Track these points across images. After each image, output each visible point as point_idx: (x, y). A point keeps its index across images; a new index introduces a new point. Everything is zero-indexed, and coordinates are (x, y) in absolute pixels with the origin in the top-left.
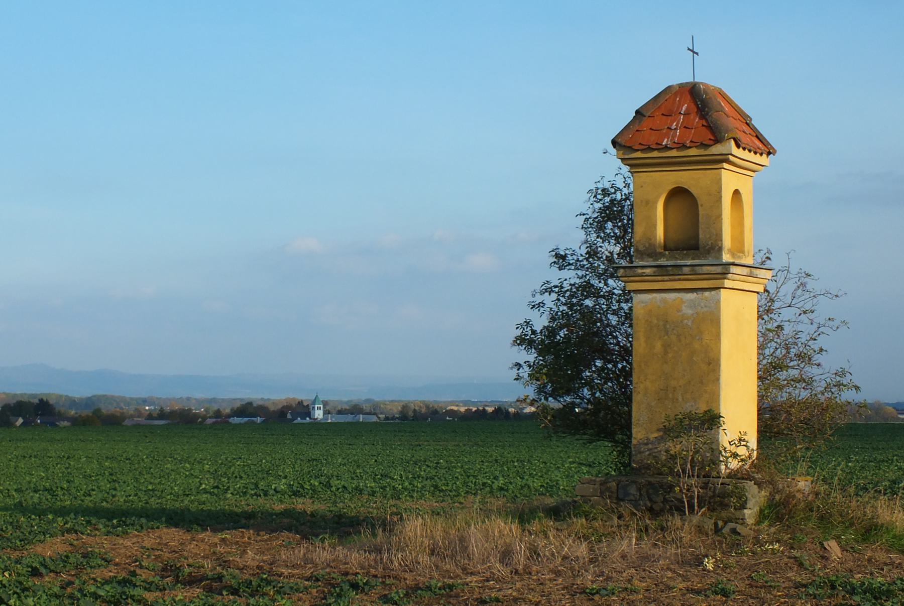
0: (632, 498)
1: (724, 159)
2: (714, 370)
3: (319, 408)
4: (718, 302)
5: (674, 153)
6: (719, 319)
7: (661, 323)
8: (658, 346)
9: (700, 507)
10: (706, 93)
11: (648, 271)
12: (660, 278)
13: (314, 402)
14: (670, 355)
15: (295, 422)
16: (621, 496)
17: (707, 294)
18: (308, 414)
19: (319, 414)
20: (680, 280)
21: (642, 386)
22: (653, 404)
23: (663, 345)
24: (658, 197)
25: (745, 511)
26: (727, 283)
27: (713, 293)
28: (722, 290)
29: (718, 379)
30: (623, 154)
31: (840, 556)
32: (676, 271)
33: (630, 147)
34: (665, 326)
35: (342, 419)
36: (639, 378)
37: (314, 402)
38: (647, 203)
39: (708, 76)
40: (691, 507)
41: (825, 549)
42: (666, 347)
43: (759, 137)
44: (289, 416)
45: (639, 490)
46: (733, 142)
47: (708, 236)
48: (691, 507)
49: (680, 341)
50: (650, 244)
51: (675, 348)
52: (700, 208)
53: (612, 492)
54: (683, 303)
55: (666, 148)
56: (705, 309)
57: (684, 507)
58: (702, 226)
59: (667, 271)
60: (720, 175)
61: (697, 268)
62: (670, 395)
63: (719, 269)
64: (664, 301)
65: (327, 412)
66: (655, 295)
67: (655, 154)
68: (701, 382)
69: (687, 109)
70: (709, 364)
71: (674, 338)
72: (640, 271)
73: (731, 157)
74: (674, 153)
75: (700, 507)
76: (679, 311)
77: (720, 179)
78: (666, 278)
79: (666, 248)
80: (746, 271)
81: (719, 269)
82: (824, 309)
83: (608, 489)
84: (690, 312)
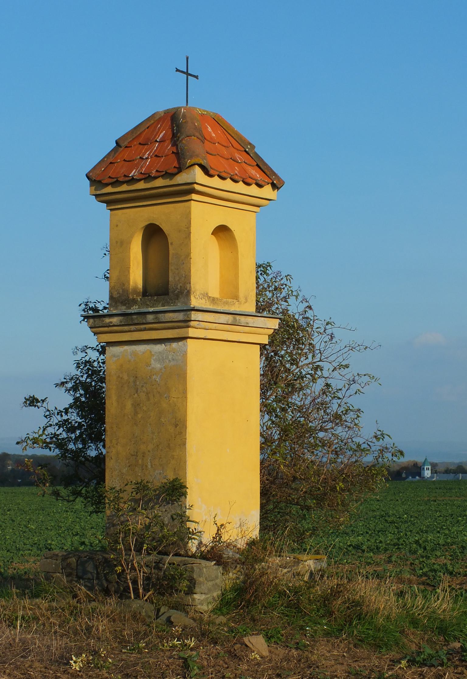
0: (89, 576)
1: (188, 190)
2: (180, 433)
3: (428, 469)
4: (185, 354)
5: (141, 185)
6: (185, 374)
7: (132, 379)
8: (129, 405)
9: (146, 590)
10: (184, 116)
11: (115, 320)
12: (126, 328)
13: (424, 464)
14: (140, 416)
15: (408, 480)
16: (80, 574)
17: (174, 345)
18: (419, 474)
19: (427, 473)
20: (145, 330)
21: (114, 451)
22: (124, 471)
23: (133, 405)
24: (132, 237)
25: (195, 596)
26: (191, 332)
27: (180, 343)
28: (188, 340)
29: (184, 444)
30: (96, 190)
31: (266, 653)
32: (140, 319)
33: (100, 182)
34: (135, 382)
35: (445, 477)
36: (111, 441)
37: (424, 464)
38: (122, 243)
39: (202, 100)
40: (136, 590)
41: (246, 646)
42: (136, 405)
43: (261, 166)
44: (404, 475)
45: (96, 567)
46: (197, 169)
47: (177, 278)
48: (136, 590)
49: (148, 399)
50: (124, 290)
51: (144, 408)
52: (170, 247)
53: (72, 569)
54: (151, 356)
55: (133, 181)
56: (172, 363)
57: (130, 589)
58: (172, 268)
59: (132, 319)
60: (190, 208)
61: (160, 315)
62: (140, 461)
63: (180, 316)
64: (134, 354)
65: (434, 471)
66: (126, 348)
67: (124, 188)
68: (169, 446)
69: (163, 137)
70: (176, 426)
71: (143, 396)
72: (107, 320)
73: (197, 187)
74: (141, 185)
75: (146, 590)
76: (148, 365)
77: (190, 213)
78: (133, 328)
79: (145, 293)
80: (229, 318)
81: (180, 316)
82: (358, 363)
83: (69, 565)
84: (158, 366)
